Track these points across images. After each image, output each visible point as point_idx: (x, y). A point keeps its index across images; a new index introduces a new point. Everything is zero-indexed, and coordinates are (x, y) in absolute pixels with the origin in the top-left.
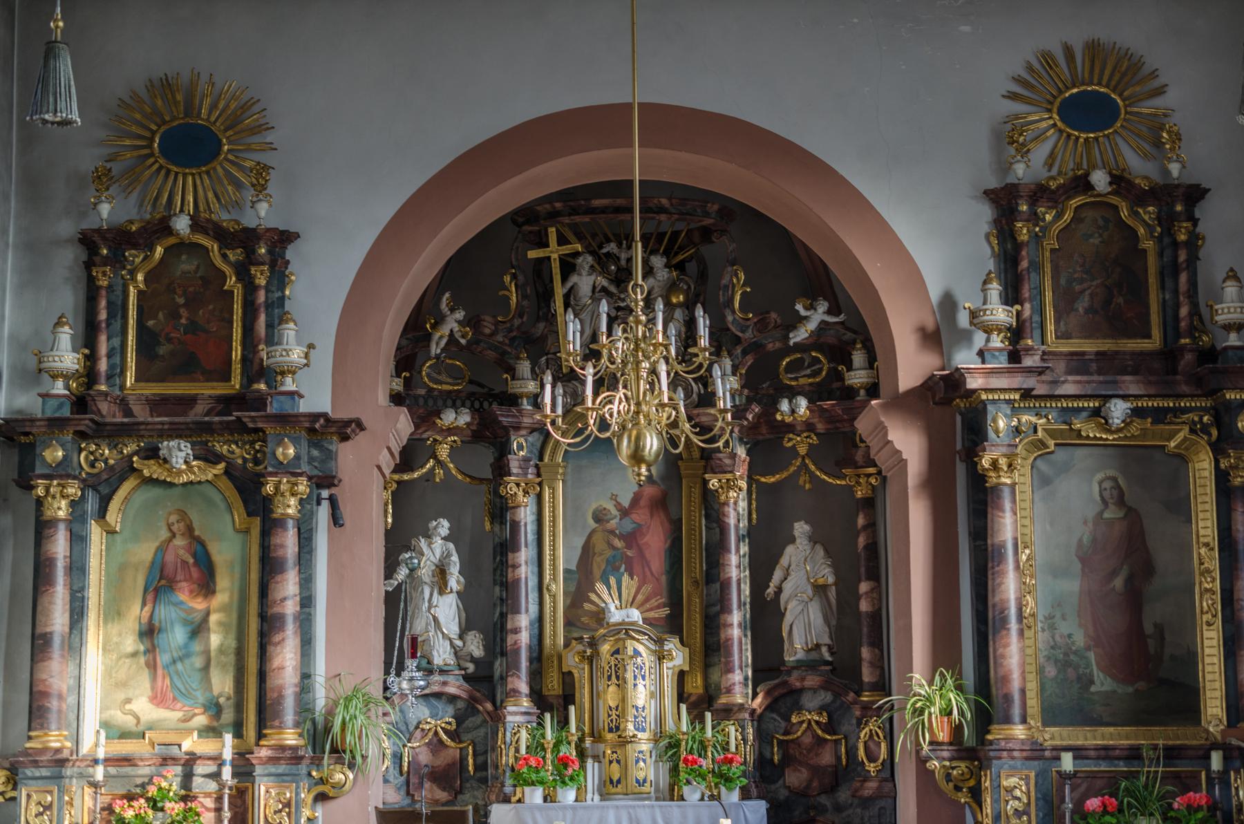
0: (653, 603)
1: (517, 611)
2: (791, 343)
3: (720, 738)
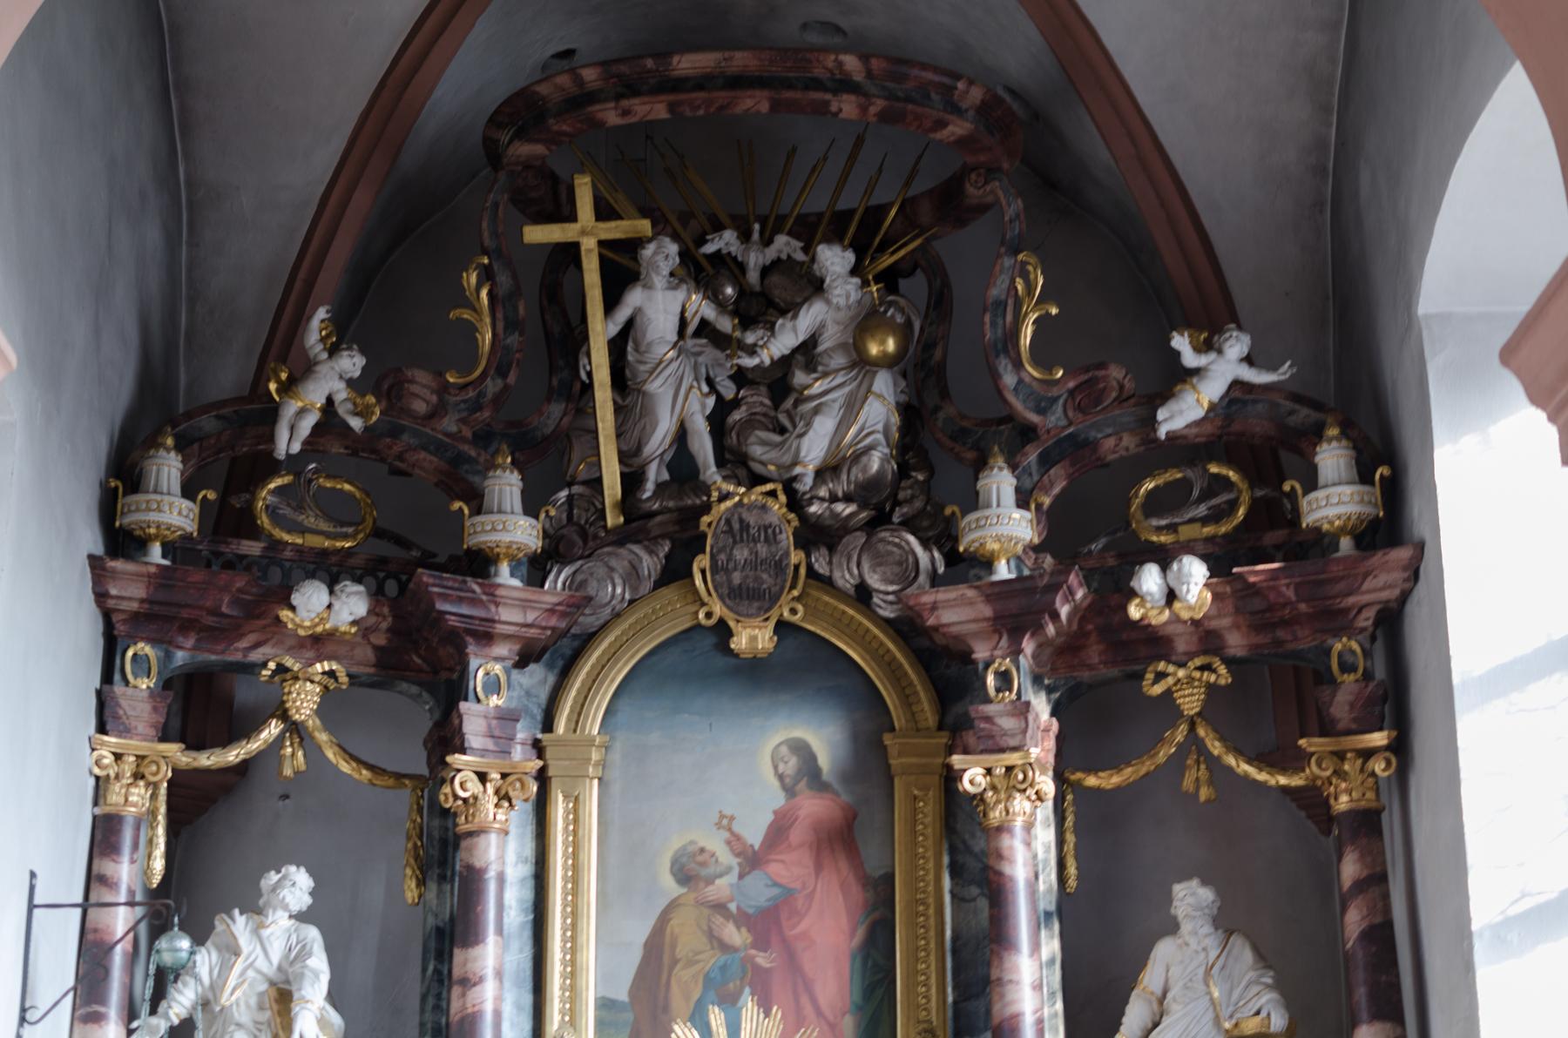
2: (1162, 432)
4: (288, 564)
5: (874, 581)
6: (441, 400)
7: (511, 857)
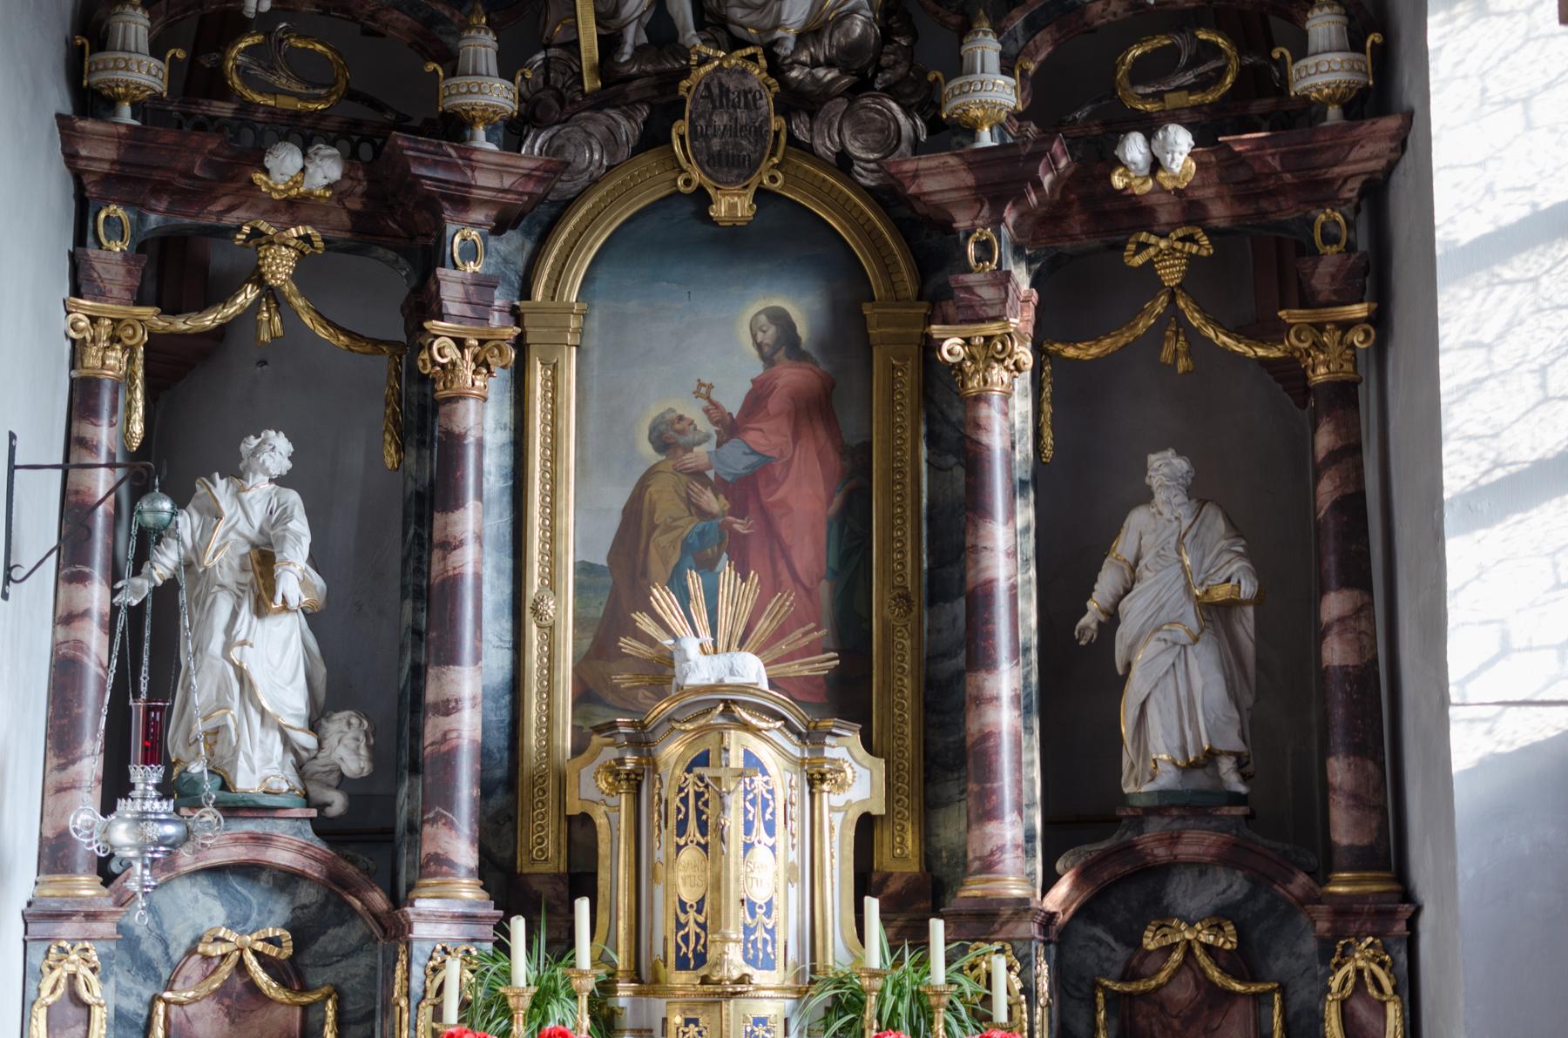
0: (797, 638)
1: (450, 657)
3: (968, 988)
4: (260, 126)
5: (855, 148)
7: (490, 423)
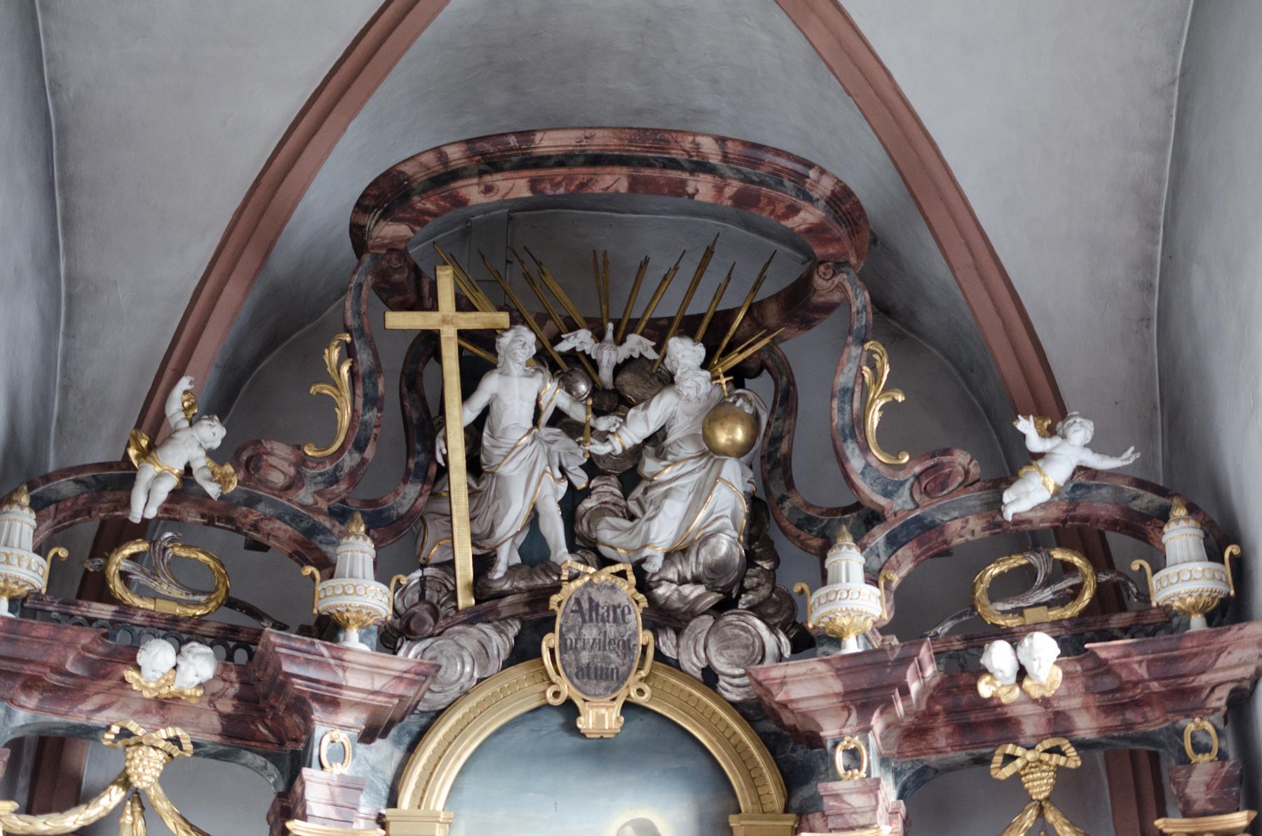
2: (1009, 514)
4: (137, 630)
5: (720, 664)
6: (298, 472)
